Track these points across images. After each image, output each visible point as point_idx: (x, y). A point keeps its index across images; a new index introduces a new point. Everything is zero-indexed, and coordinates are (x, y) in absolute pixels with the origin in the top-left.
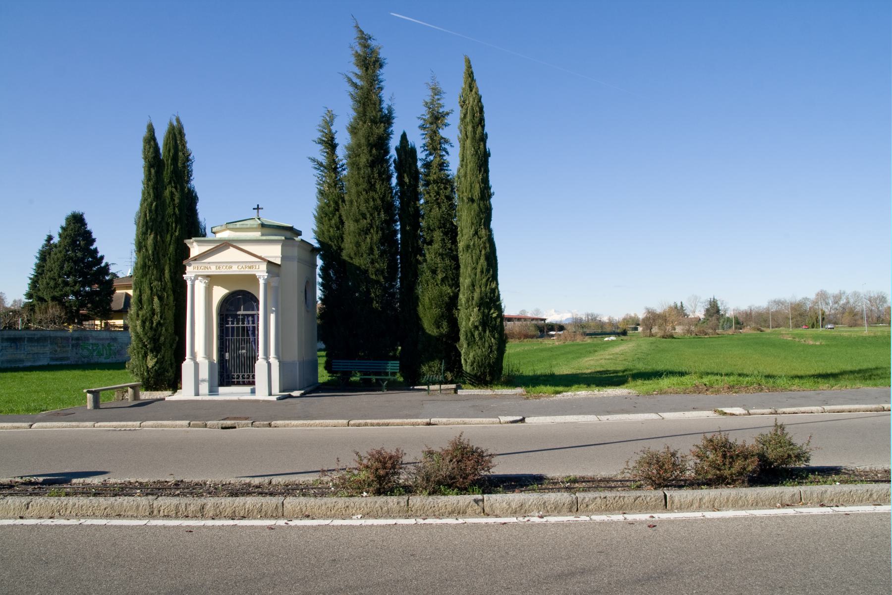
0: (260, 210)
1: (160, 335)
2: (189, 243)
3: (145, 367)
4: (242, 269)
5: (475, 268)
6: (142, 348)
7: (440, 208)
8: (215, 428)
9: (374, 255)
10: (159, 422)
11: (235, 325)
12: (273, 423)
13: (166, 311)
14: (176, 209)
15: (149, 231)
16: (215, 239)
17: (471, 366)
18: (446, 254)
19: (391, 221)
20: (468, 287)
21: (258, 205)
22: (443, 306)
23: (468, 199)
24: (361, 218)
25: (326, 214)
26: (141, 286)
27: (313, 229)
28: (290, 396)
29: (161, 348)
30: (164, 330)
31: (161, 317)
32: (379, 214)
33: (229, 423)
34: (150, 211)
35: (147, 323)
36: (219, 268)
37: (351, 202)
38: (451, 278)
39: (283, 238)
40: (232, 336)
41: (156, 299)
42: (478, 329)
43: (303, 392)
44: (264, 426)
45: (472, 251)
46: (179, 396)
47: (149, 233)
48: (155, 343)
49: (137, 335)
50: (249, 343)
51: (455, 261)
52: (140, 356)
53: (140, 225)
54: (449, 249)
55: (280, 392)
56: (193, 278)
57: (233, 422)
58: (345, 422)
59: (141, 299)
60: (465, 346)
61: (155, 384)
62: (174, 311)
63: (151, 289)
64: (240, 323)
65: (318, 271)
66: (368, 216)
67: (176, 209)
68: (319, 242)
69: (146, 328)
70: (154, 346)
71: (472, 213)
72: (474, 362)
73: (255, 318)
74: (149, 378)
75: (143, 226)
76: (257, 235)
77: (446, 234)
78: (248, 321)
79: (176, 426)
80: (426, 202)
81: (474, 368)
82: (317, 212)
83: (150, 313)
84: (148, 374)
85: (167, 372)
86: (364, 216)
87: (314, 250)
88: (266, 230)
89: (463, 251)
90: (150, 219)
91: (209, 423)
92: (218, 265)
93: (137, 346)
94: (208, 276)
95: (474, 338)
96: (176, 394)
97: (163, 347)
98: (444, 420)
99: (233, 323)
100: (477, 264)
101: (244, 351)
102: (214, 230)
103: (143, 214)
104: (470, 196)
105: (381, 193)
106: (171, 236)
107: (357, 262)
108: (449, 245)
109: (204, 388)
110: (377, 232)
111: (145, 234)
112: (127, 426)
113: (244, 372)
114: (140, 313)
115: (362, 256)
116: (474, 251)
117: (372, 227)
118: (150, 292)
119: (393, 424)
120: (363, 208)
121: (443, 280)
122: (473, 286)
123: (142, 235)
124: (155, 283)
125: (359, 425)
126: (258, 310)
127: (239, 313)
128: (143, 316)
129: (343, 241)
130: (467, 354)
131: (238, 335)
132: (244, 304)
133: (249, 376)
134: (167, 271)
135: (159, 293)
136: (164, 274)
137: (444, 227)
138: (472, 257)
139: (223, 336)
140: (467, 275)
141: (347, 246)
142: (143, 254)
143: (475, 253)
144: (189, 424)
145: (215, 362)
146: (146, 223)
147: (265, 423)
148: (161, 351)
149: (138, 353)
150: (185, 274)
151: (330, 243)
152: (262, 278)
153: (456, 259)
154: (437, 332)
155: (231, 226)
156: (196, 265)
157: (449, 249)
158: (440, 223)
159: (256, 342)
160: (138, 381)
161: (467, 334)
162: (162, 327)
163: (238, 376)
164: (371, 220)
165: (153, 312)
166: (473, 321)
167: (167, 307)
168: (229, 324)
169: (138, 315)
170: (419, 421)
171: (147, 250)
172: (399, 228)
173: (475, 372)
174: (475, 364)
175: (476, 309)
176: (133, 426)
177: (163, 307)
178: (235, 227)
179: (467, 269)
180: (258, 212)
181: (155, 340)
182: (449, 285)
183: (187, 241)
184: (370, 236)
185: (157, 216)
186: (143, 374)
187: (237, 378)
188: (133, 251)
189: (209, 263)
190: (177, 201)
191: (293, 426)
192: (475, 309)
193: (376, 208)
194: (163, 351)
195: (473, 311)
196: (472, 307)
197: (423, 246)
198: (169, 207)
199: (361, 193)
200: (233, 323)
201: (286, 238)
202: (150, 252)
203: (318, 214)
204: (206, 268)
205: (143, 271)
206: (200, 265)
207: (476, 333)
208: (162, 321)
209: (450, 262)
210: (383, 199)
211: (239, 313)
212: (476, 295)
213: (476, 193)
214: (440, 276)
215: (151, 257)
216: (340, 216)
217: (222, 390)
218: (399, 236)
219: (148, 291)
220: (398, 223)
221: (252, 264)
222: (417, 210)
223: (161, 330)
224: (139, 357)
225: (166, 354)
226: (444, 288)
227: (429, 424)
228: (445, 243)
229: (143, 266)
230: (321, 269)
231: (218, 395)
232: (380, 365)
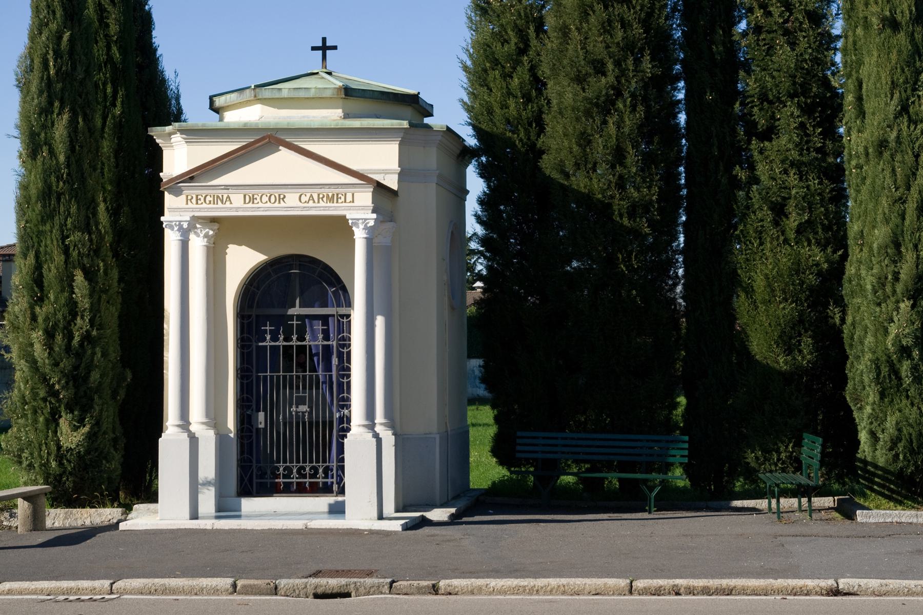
1: (89, 368)
2: (159, 137)
3: (53, 448)
4: (311, 204)
5: (902, 200)
6: (44, 400)
7: (793, 44)
8: (298, 596)
9: (625, 167)
10: (159, 581)
11: (281, 343)
12: (443, 584)
13: (103, 306)
14: (114, 49)
15: (57, 104)
16: (220, 125)
17: (891, 449)
18: (810, 163)
19: (664, 81)
20: (883, 248)
21: (324, 40)
22: (803, 297)
23: (884, 20)
24: (591, 71)
25: (496, 63)
26: (39, 244)
27: (462, 101)
28: (425, 522)
29: (93, 400)
30: (99, 355)
31: (92, 322)
32: (637, 62)
33: (333, 583)
34: (57, 54)
35: (59, 338)
36: (252, 200)
37: (564, 31)
38: (823, 225)
39: (405, 124)
40: (275, 369)
41: (79, 277)
42: (910, 356)
43: (453, 510)
44: (420, 591)
45: (892, 156)
46: (837, 497)
47: (56, 111)
48: (76, 387)
49: (33, 363)
50: (317, 388)
51: (833, 180)
52: (41, 419)
53: (34, 89)
54: (818, 150)
55: (397, 511)
56: (185, 225)
57: (343, 581)
58: (623, 583)
59: (41, 275)
60: (872, 395)
61: (78, 489)
62: (119, 306)
63: (66, 251)
64: (295, 337)
65: (472, 206)
66: (610, 66)
67: (114, 49)
68: (479, 133)
69: (57, 349)
70: (75, 394)
71: (894, 56)
72: (899, 439)
73: (344, 324)
74: (61, 476)
75: (41, 93)
76: (332, 116)
77: (807, 110)
78: (313, 331)
79: (200, 591)
80: (758, 29)
81: (896, 456)
82: (471, 56)
83: (65, 310)
84: (61, 464)
85: (105, 458)
86: (599, 69)
87: (465, 154)
88: (355, 104)
89: (867, 154)
90: (57, 73)
91: (283, 583)
92: (250, 192)
93: (35, 395)
94: (213, 220)
95: (899, 378)
96: (133, 514)
97: (96, 397)
98: (874, 583)
99: (275, 338)
100: (908, 188)
101: (304, 408)
102: (219, 102)
103: (37, 61)
104: (888, 13)
105: (642, 6)
106: (104, 119)
107: (579, 182)
108: (818, 142)
109: (208, 500)
110: (634, 109)
111: (46, 111)
112: (78, 591)
113: (305, 461)
114: (41, 312)
115: (594, 169)
116: (898, 157)
117: (619, 94)
118: (63, 257)
119: (743, 591)
120: (597, 47)
121: (799, 230)
122: (897, 245)
123: (40, 114)
124: (75, 237)
125: (658, 592)
126: (349, 304)
127: (291, 312)
128: (47, 319)
129: (541, 129)
130: (878, 418)
131: (288, 369)
132: (302, 294)
133: (316, 470)
134: (102, 207)
135: (85, 260)
136: (95, 214)
137: (805, 92)
138: (894, 171)
139: (248, 370)
140: (880, 218)
141: (553, 144)
142: (43, 164)
143: (903, 162)
144: (234, 586)
145: (232, 435)
146: (48, 85)
147: (424, 583)
148: (92, 407)
149: (35, 412)
151: (509, 134)
152: (362, 227)
153: (836, 174)
154: (786, 363)
155: (266, 93)
156: (193, 193)
157: (818, 150)
158: (794, 83)
159: (344, 388)
160: (35, 482)
161: (878, 368)
162: (93, 348)
163: (289, 470)
164: (617, 78)
165: (73, 309)
166: (897, 336)
167: (104, 296)
168: (264, 340)
169: (34, 318)
170: (810, 583)
171: (52, 152)
172: (681, 96)
173: (900, 465)
174: (901, 446)
175: (905, 305)
176: (93, 590)
177: (96, 296)
178: (277, 95)
179: (877, 203)
180: (324, 57)
181: (76, 378)
182: (818, 243)
183: (156, 132)
184: (616, 118)
185: (74, 68)
186: (46, 465)
187: (312, 476)
189: (227, 187)
190: (114, 29)
191: (493, 592)
192: (902, 305)
193: (629, 47)
194: (97, 408)
195: (897, 309)
196: (893, 299)
197: (749, 142)
198: (97, 42)
199: (592, 7)
200: (275, 338)
201: (411, 124)
202: (62, 158)
203: (474, 63)
204: (218, 199)
205: (44, 207)
206: (205, 192)
207: (905, 368)
208: (94, 333)
209: (820, 183)
210: (646, 23)
211: (291, 312)
212: (906, 270)
213: (905, 6)
214: (793, 221)
215: (65, 171)
216: (533, 69)
217: (249, 504)
218: (682, 118)
219: (59, 258)
220: (681, 84)
221: (336, 191)
222: (731, 48)
223: (94, 354)
224: (36, 421)
225: (105, 414)
226: (805, 251)
227: (836, 592)
228: (807, 135)
229: (44, 193)
230: (481, 202)
231: (239, 517)
232: (534, 441)
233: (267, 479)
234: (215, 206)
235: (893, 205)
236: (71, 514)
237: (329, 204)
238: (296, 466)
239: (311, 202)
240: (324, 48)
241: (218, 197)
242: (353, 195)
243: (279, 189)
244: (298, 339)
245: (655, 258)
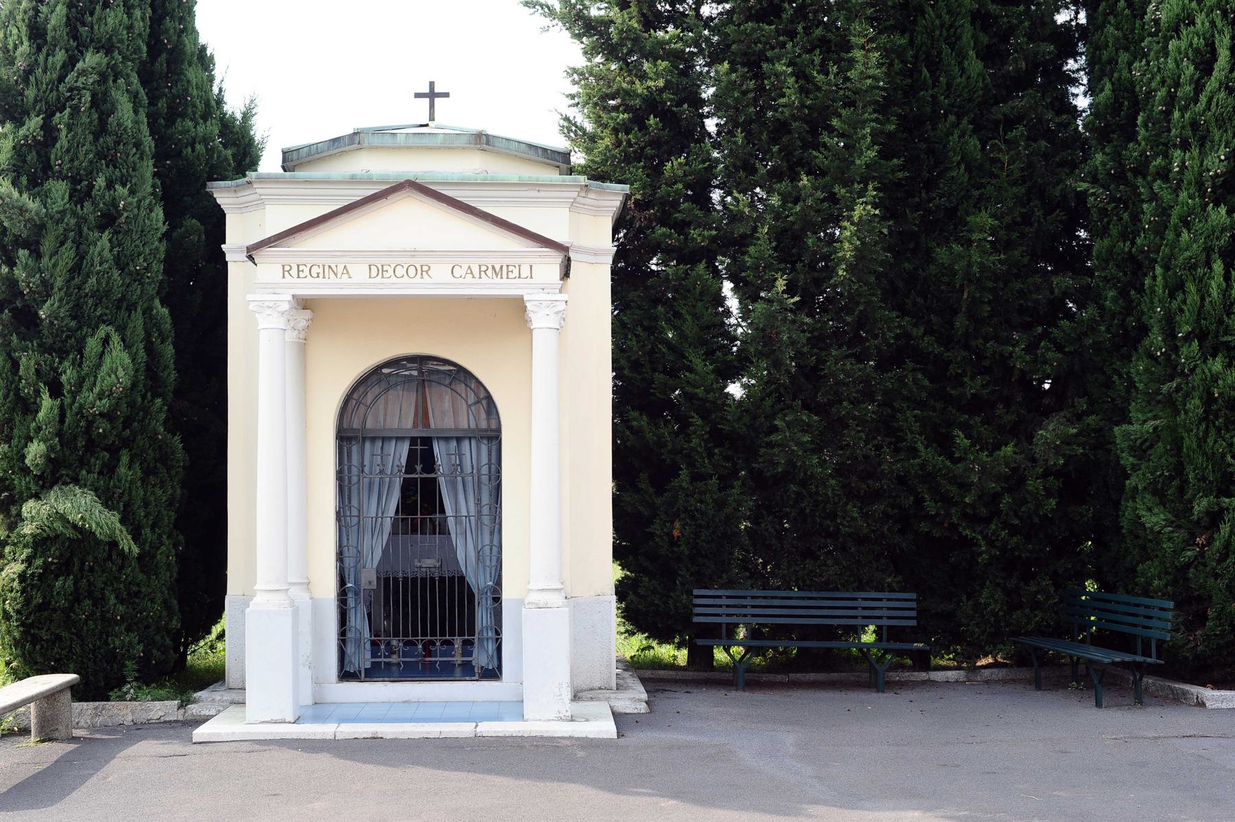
0: (437, 90)
21: (432, 84)
36: (382, 271)
64: (419, 468)
150: (225, 243)
180: (432, 106)
188: (565, 685)
233: (380, 657)
234: (326, 280)
235: (25, 420)
236: (103, 709)
237: (498, 280)
238: (422, 640)
240: (432, 95)
241: (330, 267)
242: (531, 266)
243: (419, 260)
244: (424, 470)
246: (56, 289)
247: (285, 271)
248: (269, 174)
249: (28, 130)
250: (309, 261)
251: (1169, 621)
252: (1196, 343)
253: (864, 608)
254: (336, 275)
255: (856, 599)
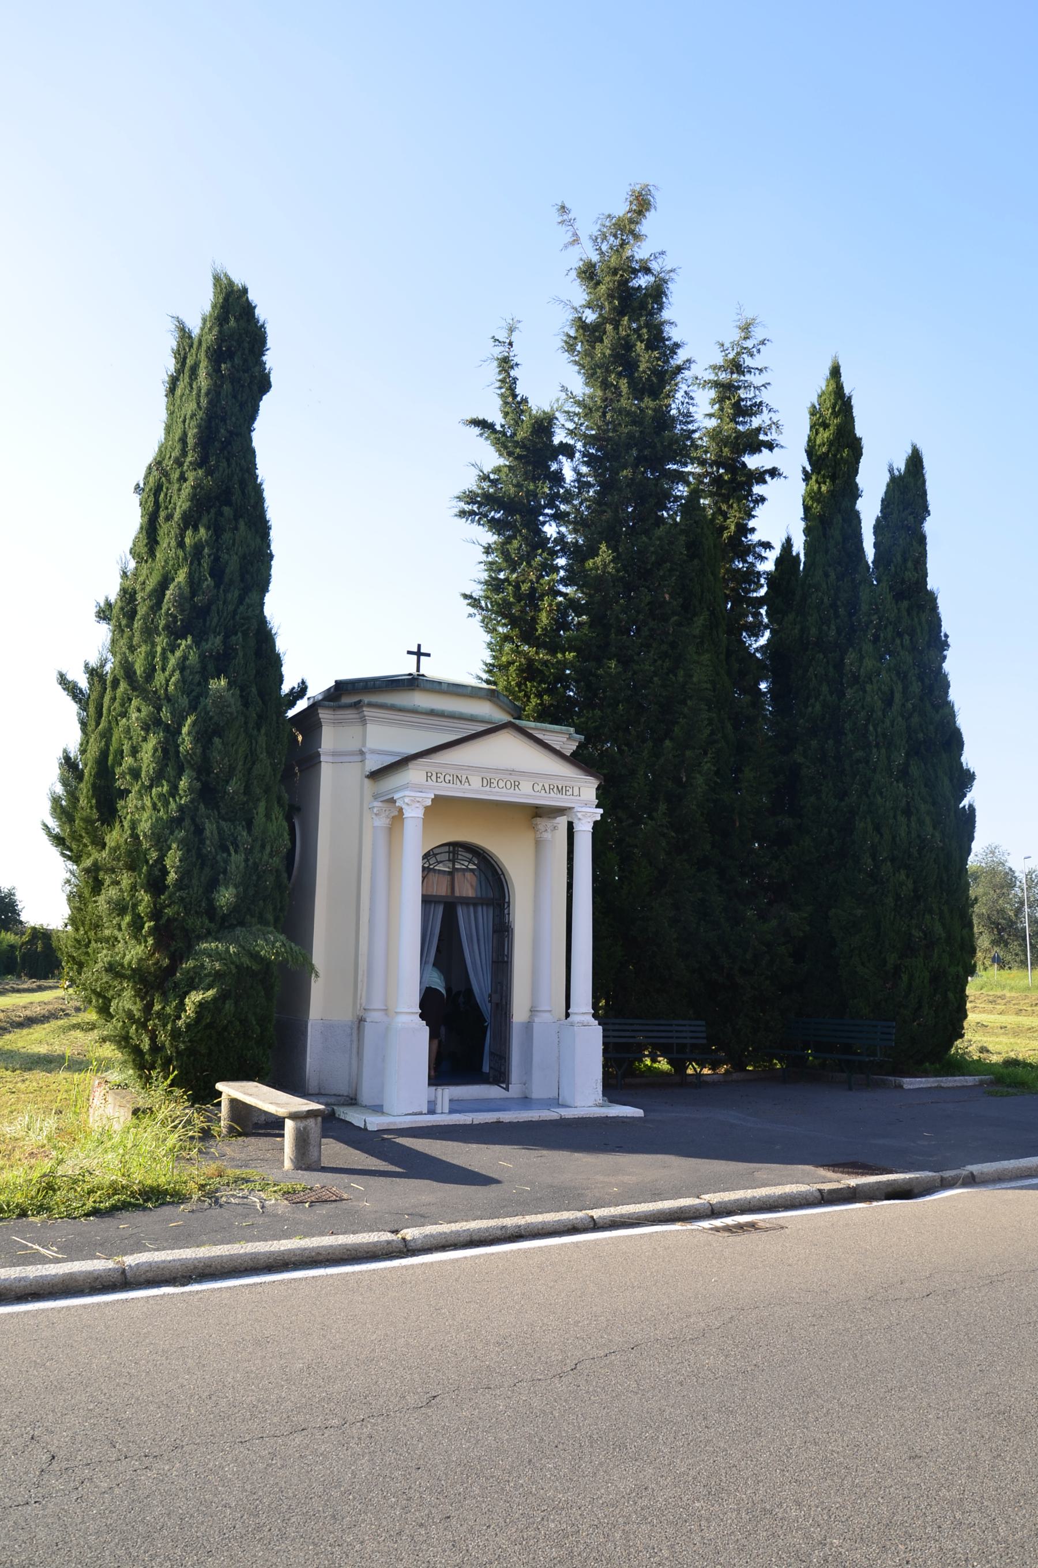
21: (419, 646)
234: (454, 786)
237: (559, 796)
239: (543, 791)
240: (419, 654)
243: (514, 776)
245: (749, 1051)
246: (238, 772)
247: (428, 777)
248: (472, 715)
249: (213, 644)
250: (444, 771)
251: (894, 1027)
252: (889, 863)
253: (677, 1031)
254: (461, 782)
255: (671, 1025)
